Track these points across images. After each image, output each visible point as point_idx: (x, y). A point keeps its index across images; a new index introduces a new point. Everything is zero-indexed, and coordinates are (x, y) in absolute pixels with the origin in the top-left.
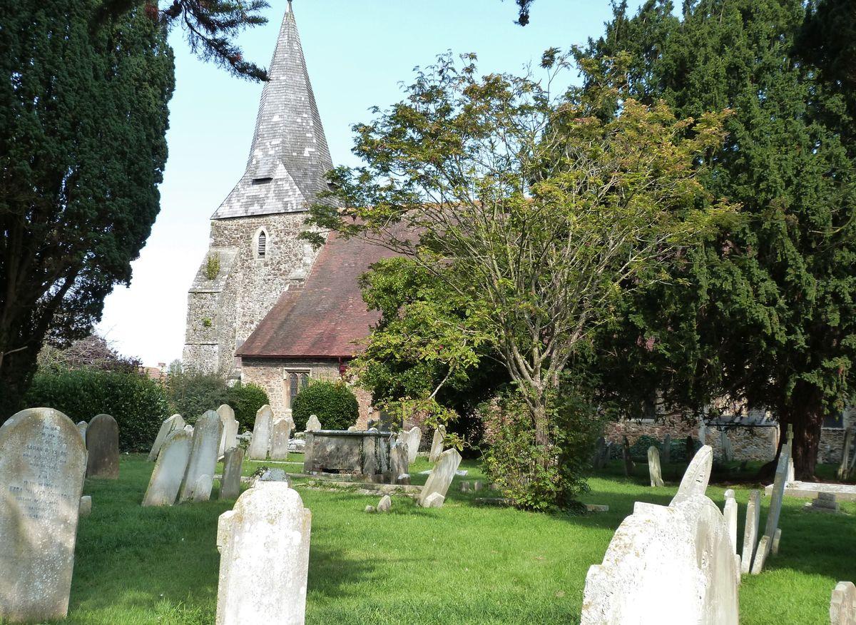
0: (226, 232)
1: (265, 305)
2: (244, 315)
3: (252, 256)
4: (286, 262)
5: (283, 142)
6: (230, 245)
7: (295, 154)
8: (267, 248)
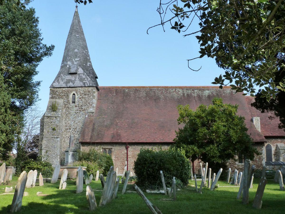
0: (57, 93)
1: (76, 122)
2: (66, 126)
3: (69, 103)
4: (85, 106)
5: (80, 60)
6: (59, 98)
7: (84, 65)
8: (76, 100)
